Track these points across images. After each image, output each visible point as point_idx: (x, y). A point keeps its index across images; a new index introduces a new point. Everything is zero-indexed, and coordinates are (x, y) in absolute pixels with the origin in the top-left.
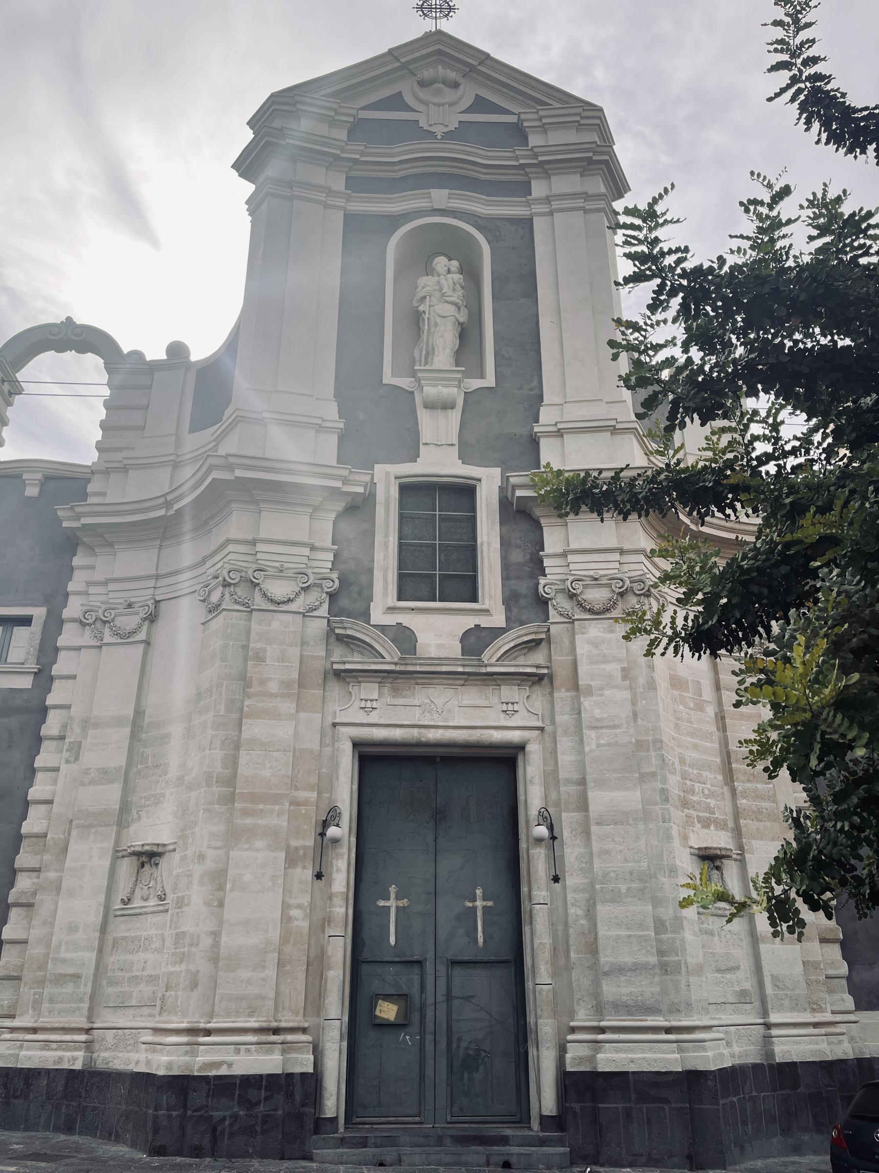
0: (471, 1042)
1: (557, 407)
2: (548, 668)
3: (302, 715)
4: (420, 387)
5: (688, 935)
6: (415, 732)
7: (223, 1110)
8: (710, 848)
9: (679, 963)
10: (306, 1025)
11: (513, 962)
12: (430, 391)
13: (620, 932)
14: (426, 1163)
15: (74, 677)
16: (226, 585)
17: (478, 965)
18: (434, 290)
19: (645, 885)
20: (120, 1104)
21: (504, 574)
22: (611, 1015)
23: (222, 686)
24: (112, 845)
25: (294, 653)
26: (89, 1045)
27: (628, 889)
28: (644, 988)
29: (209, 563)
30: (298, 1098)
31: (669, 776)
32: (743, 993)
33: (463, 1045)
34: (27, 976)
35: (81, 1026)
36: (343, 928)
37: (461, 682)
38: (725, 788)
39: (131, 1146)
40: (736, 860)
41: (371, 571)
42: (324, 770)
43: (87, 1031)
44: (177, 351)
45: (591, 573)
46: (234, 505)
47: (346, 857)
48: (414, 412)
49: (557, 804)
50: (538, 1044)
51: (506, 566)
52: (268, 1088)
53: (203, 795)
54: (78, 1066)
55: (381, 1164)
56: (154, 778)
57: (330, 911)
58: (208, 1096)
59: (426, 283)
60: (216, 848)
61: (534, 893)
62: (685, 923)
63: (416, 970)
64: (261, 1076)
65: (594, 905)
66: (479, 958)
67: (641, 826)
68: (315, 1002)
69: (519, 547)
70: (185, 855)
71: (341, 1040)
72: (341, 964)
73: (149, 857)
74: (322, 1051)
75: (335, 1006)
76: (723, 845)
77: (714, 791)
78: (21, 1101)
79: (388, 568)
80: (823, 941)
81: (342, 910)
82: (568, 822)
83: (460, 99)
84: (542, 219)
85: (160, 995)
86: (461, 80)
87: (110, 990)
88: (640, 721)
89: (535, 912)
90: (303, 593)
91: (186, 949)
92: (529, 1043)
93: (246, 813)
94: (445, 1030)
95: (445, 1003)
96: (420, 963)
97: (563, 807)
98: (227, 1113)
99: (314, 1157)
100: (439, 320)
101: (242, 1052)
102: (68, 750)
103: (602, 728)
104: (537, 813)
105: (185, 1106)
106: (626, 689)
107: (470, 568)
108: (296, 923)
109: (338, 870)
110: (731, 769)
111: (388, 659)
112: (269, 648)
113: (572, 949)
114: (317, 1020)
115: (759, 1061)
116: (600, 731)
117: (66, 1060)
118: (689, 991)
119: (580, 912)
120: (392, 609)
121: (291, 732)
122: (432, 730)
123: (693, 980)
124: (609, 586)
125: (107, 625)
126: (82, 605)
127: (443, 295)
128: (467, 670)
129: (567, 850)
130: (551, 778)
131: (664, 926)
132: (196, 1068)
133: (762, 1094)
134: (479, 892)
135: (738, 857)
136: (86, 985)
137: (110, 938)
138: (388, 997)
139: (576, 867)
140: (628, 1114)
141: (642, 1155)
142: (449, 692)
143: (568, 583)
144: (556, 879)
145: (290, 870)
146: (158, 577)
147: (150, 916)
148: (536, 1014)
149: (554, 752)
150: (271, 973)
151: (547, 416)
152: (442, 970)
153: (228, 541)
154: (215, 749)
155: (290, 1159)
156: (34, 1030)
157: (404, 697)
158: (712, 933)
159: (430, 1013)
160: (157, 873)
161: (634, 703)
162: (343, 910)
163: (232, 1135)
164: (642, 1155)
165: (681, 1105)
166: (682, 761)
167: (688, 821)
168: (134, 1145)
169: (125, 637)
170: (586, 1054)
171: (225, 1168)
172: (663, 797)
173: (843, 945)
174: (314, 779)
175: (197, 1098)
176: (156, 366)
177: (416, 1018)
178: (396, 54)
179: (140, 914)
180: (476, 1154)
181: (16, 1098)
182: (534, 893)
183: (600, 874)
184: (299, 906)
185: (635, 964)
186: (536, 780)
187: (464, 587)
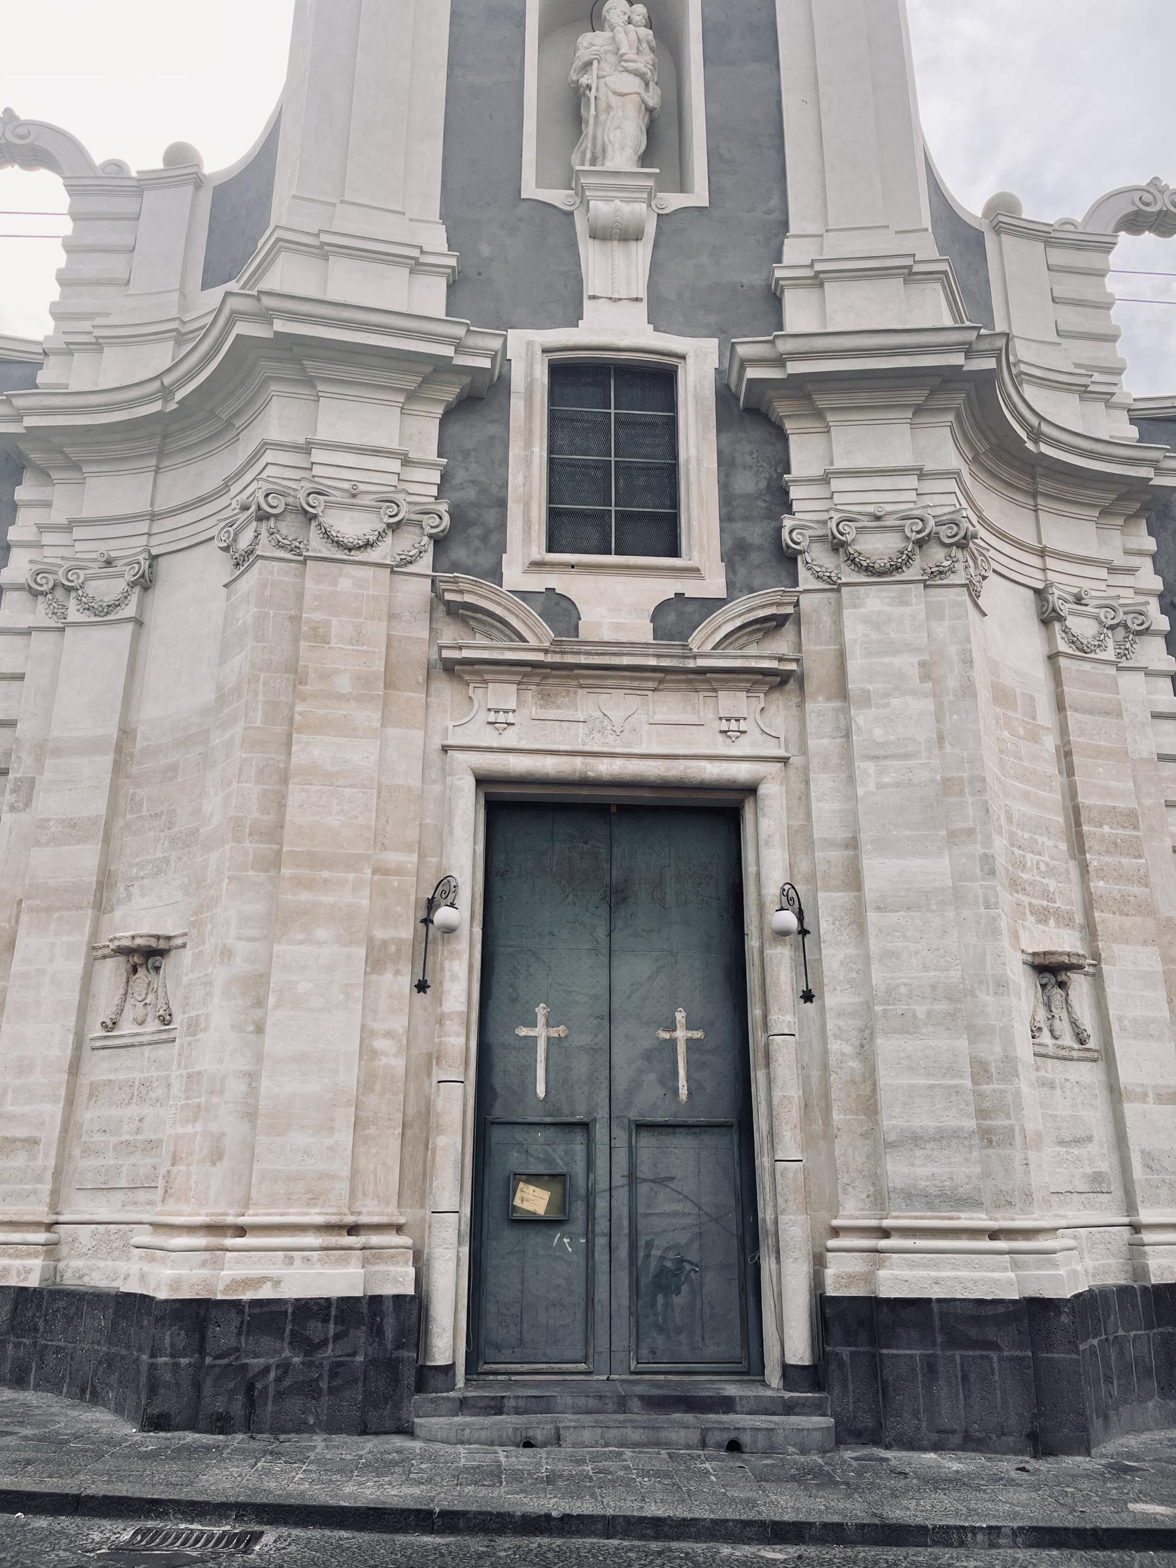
0: (668, 1248)
1: (813, 239)
2: (797, 660)
3: (391, 731)
4: (585, 203)
7: (266, 1356)
8: (1052, 953)
10: (402, 1220)
11: (734, 1123)
12: (603, 208)
13: (914, 1079)
14: (602, 1442)
15: (21, 677)
16: (262, 517)
17: (678, 1130)
18: (606, 52)
19: (957, 1008)
20: (99, 1343)
21: (724, 511)
22: (900, 1209)
23: (258, 681)
24: (86, 938)
25: (378, 630)
26: (51, 1248)
27: (929, 1014)
28: (957, 1168)
29: (235, 489)
31: (995, 837)
35: (37, 1219)
36: (462, 1069)
37: (651, 684)
39: (116, 1411)
41: (502, 503)
42: (428, 821)
43: (50, 1227)
44: (180, 158)
45: (870, 509)
46: (274, 387)
47: (466, 956)
48: (575, 245)
50: (778, 1252)
51: (727, 499)
52: (341, 1320)
53: (228, 854)
54: (33, 1281)
55: (528, 1444)
56: (151, 834)
57: (441, 1043)
58: (239, 1334)
59: (591, 42)
60: (251, 940)
64: (328, 1300)
65: (872, 1038)
67: (950, 914)
68: (416, 1182)
69: (745, 467)
70: (201, 952)
71: (459, 1244)
72: (458, 1126)
73: (148, 956)
74: (428, 1260)
75: (450, 1191)
77: (1054, 867)
79: (531, 498)
81: (459, 1041)
85: (163, 1171)
87: (85, 1163)
88: (948, 748)
90: (390, 533)
91: (203, 1100)
92: (763, 1250)
93: (299, 883)
94: (626, 1231)
95: (627, 1188)
96: (585, 1126)
97: (819, 885)
98: (271, 1361)
99: (417, 1432)
100: (614, 100)
101: (298, 1262)
102: (13, 791)
103: (886, 757)
104: (778, 892)
105: (201, 1350)
106: (927, 697)
107: (668, 502)
108: (384, 1060)
109: (454, 978)
110: (1080, 835)
111: (533, 642)
112: (334, 621)
114: (421, 1213)
115: (1123, 1282)
116: (883, 763)
117: (14, 1273)
118: (1027, 1173)
119: (848, 1049)
122: (605, 760)
124: (901, 529)
125: (73, 594)
126: (31, 562)
127: (621, 58)
128: (665, 663)
130: (801, 838)
131: (986, 1071)
132: (220, 1287)
133: (1132, 1334)
134: (680, 1016)
135: (1091, 970)
136: (46, 1155)
137: (84, 1081)
138: (534, 1179)
139: (841, 978)
141: (953, 1432)
142: (633, 701)
143: (832, 525)
144: (808, 997)
145: (374, 977)
146: (153, 517)
147: (147, 1049)
148: (775, 1206)
149: (805, 797)
150: (344, 1137)
151: (795, 253)
152: (621, 1137)
153: (265, 446)
154: (247, 782)
155: (377, 1433)
157: (558, 707)
158: (1052, 1086)
159: (601, 1204)
160: (157, 981)
162: (462, 1040)
163: (280, 1395)
164: (953, 1432)
165: (1018, 1353)
166: (1010, 819)
168: (119, 1410)
169: (103, 612)
170: (858, 1269)
171: (265, 1452)
172: (986, 868)
174: (412, 834)
175: (222, 1336)
176: (145, 184)
177: (579, 1210)
179: (133, 1046)
180: (682, 1427)
182: (773, 1017)
184: (389, 1034)
185: (940, 1130)
187: (660, 533)
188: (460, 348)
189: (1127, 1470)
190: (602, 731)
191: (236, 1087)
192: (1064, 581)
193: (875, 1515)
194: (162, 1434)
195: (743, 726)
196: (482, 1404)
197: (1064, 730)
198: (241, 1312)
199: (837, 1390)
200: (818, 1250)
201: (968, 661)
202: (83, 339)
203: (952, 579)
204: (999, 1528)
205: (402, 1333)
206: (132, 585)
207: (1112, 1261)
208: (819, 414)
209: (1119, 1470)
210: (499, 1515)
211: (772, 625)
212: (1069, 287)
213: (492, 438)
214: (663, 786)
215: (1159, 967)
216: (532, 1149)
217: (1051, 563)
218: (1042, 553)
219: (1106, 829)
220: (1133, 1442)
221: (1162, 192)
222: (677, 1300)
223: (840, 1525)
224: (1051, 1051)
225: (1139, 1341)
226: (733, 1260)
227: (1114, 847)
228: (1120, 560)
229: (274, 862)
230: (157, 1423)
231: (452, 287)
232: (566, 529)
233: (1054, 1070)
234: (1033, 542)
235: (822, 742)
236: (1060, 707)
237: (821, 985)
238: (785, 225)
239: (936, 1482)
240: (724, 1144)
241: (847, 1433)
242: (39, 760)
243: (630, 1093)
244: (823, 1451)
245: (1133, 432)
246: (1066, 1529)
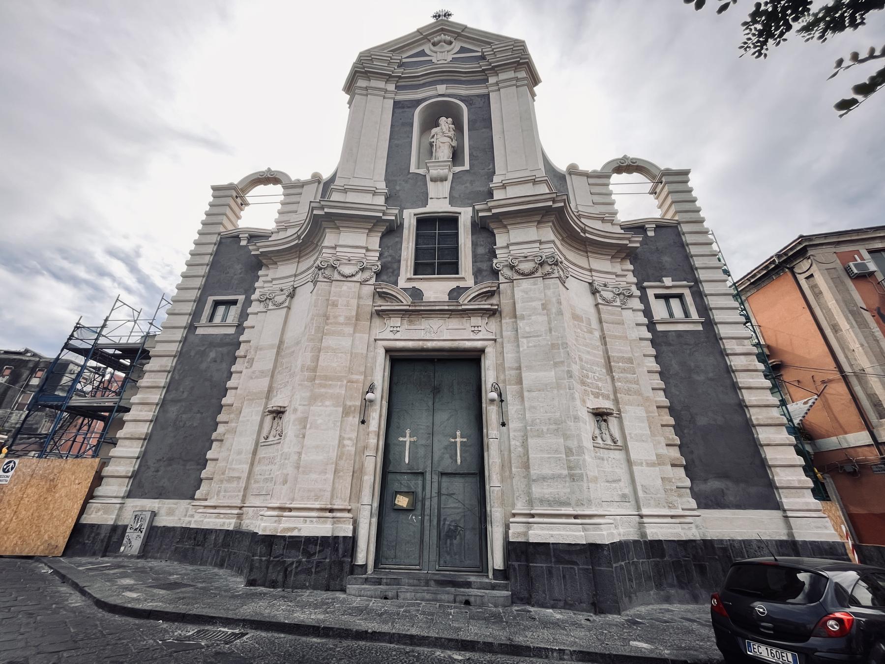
3: (357, 335)
5: (587, 457)
6: (421, 343)
12: (434, 172)
13: (544, 456)
16: (320, 269)
25: (354, 302)
28: (559, 490)
30: (341, 551)
32: (624, 496)
33: (447, 523)
34: (216, 478)
38: (608, 377)
41: (399, 261)
46: (327, 230)
47: (378, 411)
49: (504, 381)
52: (321, 545)
54: (231, 528)
55: (386, 598)
62: (585, 451)
63: (420, 478)
66: (457, 472)
67: (555, 392)
68: (356, 494)
69: (481, 245)
73: (278, 413)
80: (673, 465)
82: (510, 393)
84: (494, 93)
86: (453, 40)
93: (321, 386)
109: (373, 419)
110: (610, 366)
113: (513, 465)
119: (518, 444)
120: (409, 279)
121: (350, 343)
124: (534, 260)
127: (443, 133)
129: (510, 407)
130: (500, 367)
134: (458, 433)
137: (257, 457)
138: (401, 493)
140: (550, 571)
142: (441, 322)
144: (503, 424)
146: (295, 276)
150: (330, 476)
151: (496, 179)
156: (215, 507)
158: (603, 459)
159: (427, 503)
161: (549, 323)
162: (375, 441)
163: (296, 574)
169: (278, 306)
173: (686, 468)
174: (362, 369)
175: (278, 549)
184: (349, 439)
185: (553, 474)
186: (491, 368)
187: (452, 267)
188: (384, 214)
191: (295, 457)
192: (599, 280)
193: (509, 639)
195: (480, 329)
197: (602, 330)
198: (285, 540)
202: (282, 226)
203: (553, 276)
205: (345, 551)
206: (288, 296)
208: (505, 227)
209: (633, 623)
210: (346, 630)
211: (490, 294)
217: (594, 274)
218: (591, 270)
222: (455, 542)
224: (602, 446)
225: (645, 564)
226: (477, 526)
227: (624, 370)
228: (619, 272)
230: (251, 583)
232: (420, 268)
233: (603, 453)
235: (508, 333)
236: (601, 321)
238: (494, 173)
239: (547, 624)
240: (474, 481)
241: (516, 599)
243: (439, 461)
246: (596, 653)
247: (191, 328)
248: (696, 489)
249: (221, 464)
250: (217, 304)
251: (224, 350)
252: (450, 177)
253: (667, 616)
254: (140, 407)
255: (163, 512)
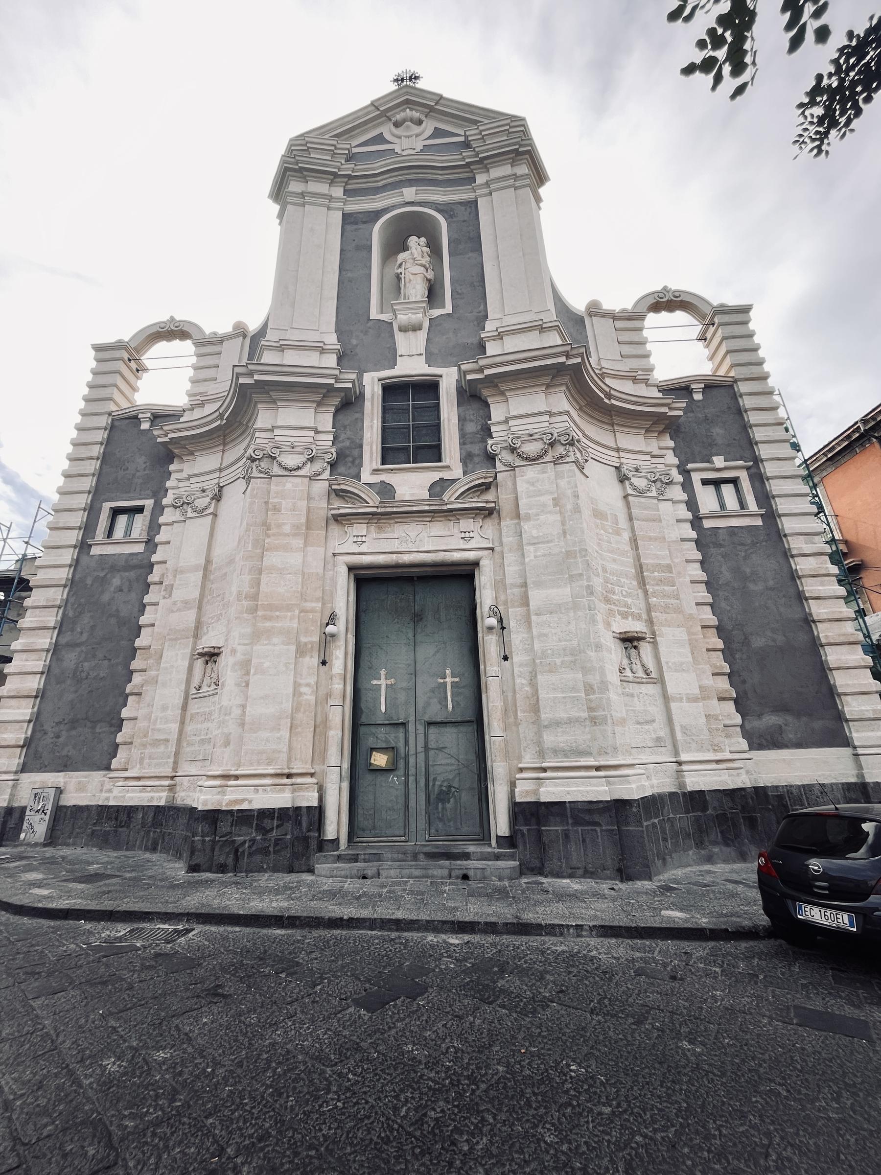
6: (394, 556)
7: (243, 836)
9: (605, 718)
10: (313, 771)
12: (403, 318)
13: (556, 693)
15: (169, 543)
19: (576, 658)
25: (303, 504)
26: (172, 788)
27: (562, 662)
28: (579, 736)
30: (304, 824)
32: (658, 739)
33: (438, 783)
34: (137, 741)
36: (341, 700)
37: (428, 519)
38: (640, 591)
40: (649, 642)
41: (361, 446)
45: (527, 432)
47: (343, 648)
48: (393, 336)
49: (506, 603)
51: (463, 435)
52: (280, 818)
54: (162, 803)
55: (364, 877)
58: (232, 826)
60: (245, 645)
61: (488, 668)
62: (610, 686)
63: (401, 730)
64: (274, 809)
67: (572, 614)
68: (319, 752)
69: (471, 421)
73: (211, 656)
76: (638, 630)
78: (125, 829)
80: (721, 699)
83: (423, 132)
86: (423, 117)
87: (188, 749)
88: (568, 537)
89: (489, 682)
93: (266, 618)
96: (404, 724)
100: (412, 277)
101: (260, 792)
107: (436, 439)
108: (305, 697)
109: (337, 658)
110: (643, 577)
112: (284, 502)
113: (519, 709)
120: (376, 471)
122: (407, 555)
123: (618, 729)
124: (542, 439)
127: (414, 259)
130: (500, 585)
134: (448, 672)
135: (652, 640)
141: (579, 868)
142: (420, 527)
144: (506, 658)
146: (221, 470)
149: (502, 565)
150: (285, 733)
151: (490, 326)
155: (298, 872)
156: (138, 778)
159: (412, 760)
161: (563, 523)
162: (342, 686)
164: (579, 868)
165: (610, 828)
167: (611, 613)
174: (319, 594)
175: (224, 827)
178: (376, 104)
181: (122, 827)
183: (540, 652)
184: (308, 685)
185: (569, 719)
186: (488, 586)
187: (431, 452)
188: (337, 380)
189: (670, 889)
190: (406, 541)
191: (236, 712)
192: (629, 462)
194: (195, 874)
195: (472, 534)
196: (348, 857)
197: (633, 529)
198: (233, 815)
199: (521, 848)
200: (513, 779)
201: (577, 497)
203: (568, 460)
204: (582, 926)
205: (310, 824)
206: (212, 499)
207: (668, 780)
208: (502, 393)
209: (667, 889)
212: (626, 336)
213: (357, 419)
214: (435, 565)
215: (685, 637)
216: (379, 736)
217: (622, 454)
218: (618, 450)
219: (656, 574)
220: (680, 873)
221: (668, 292)
222: (448, 806)
223: (495, 924)
224: (631, 679)
225: (683, 819)
227: (660, 582)
228: (656, 451)
229: (254, 610)
231: (340, 359)
232: (388, 455)
234: (613, 445)
235: (509, 539)
236: (631, 519)
237: (511, 652)
238: (486, 317)
239: (561, 896)
241: (524, 869)
242: (175, 576)
243: (424, 708)
244: (511, 879)
245: (660, 395)
246: (620, 927)
247: (84, 546)
248: (748, 726)
249: (141, 724)
250: (116, 512)
251: (132, 574)
252: (426, 325)
253: (708, 879)
254: (24, 656)
255: (71, 787)
